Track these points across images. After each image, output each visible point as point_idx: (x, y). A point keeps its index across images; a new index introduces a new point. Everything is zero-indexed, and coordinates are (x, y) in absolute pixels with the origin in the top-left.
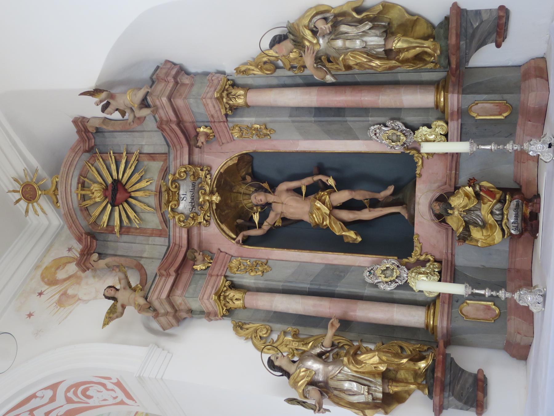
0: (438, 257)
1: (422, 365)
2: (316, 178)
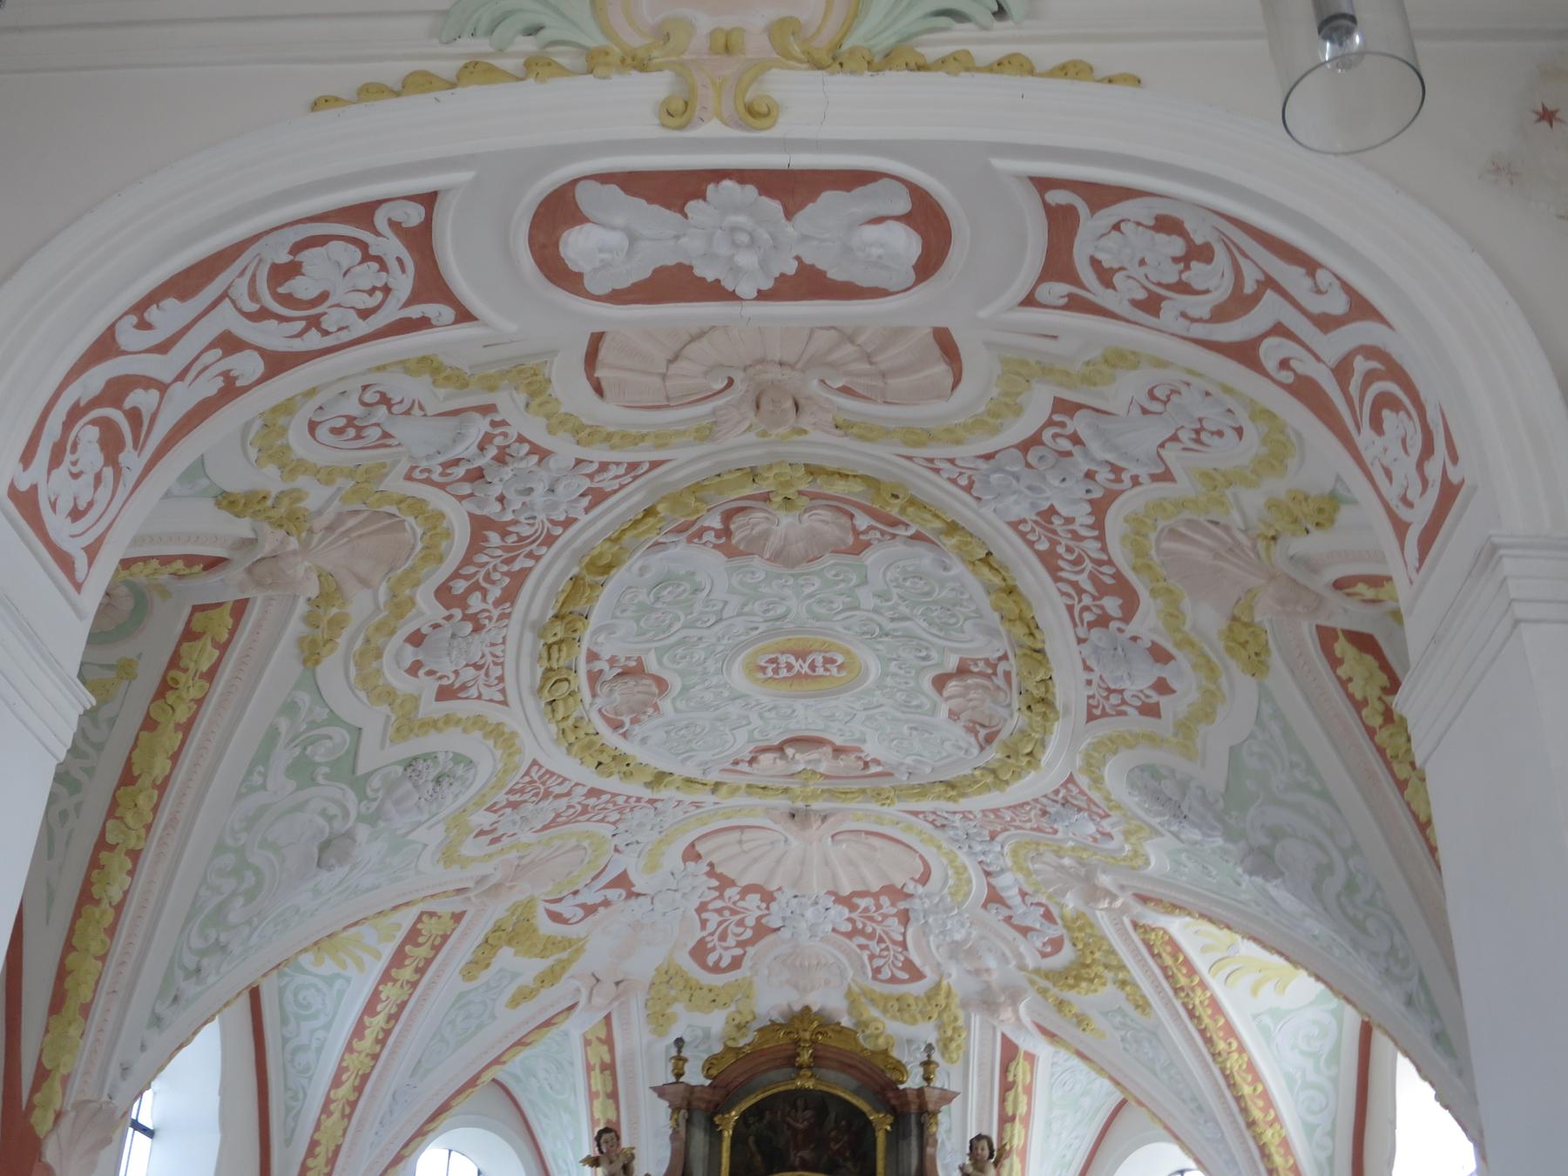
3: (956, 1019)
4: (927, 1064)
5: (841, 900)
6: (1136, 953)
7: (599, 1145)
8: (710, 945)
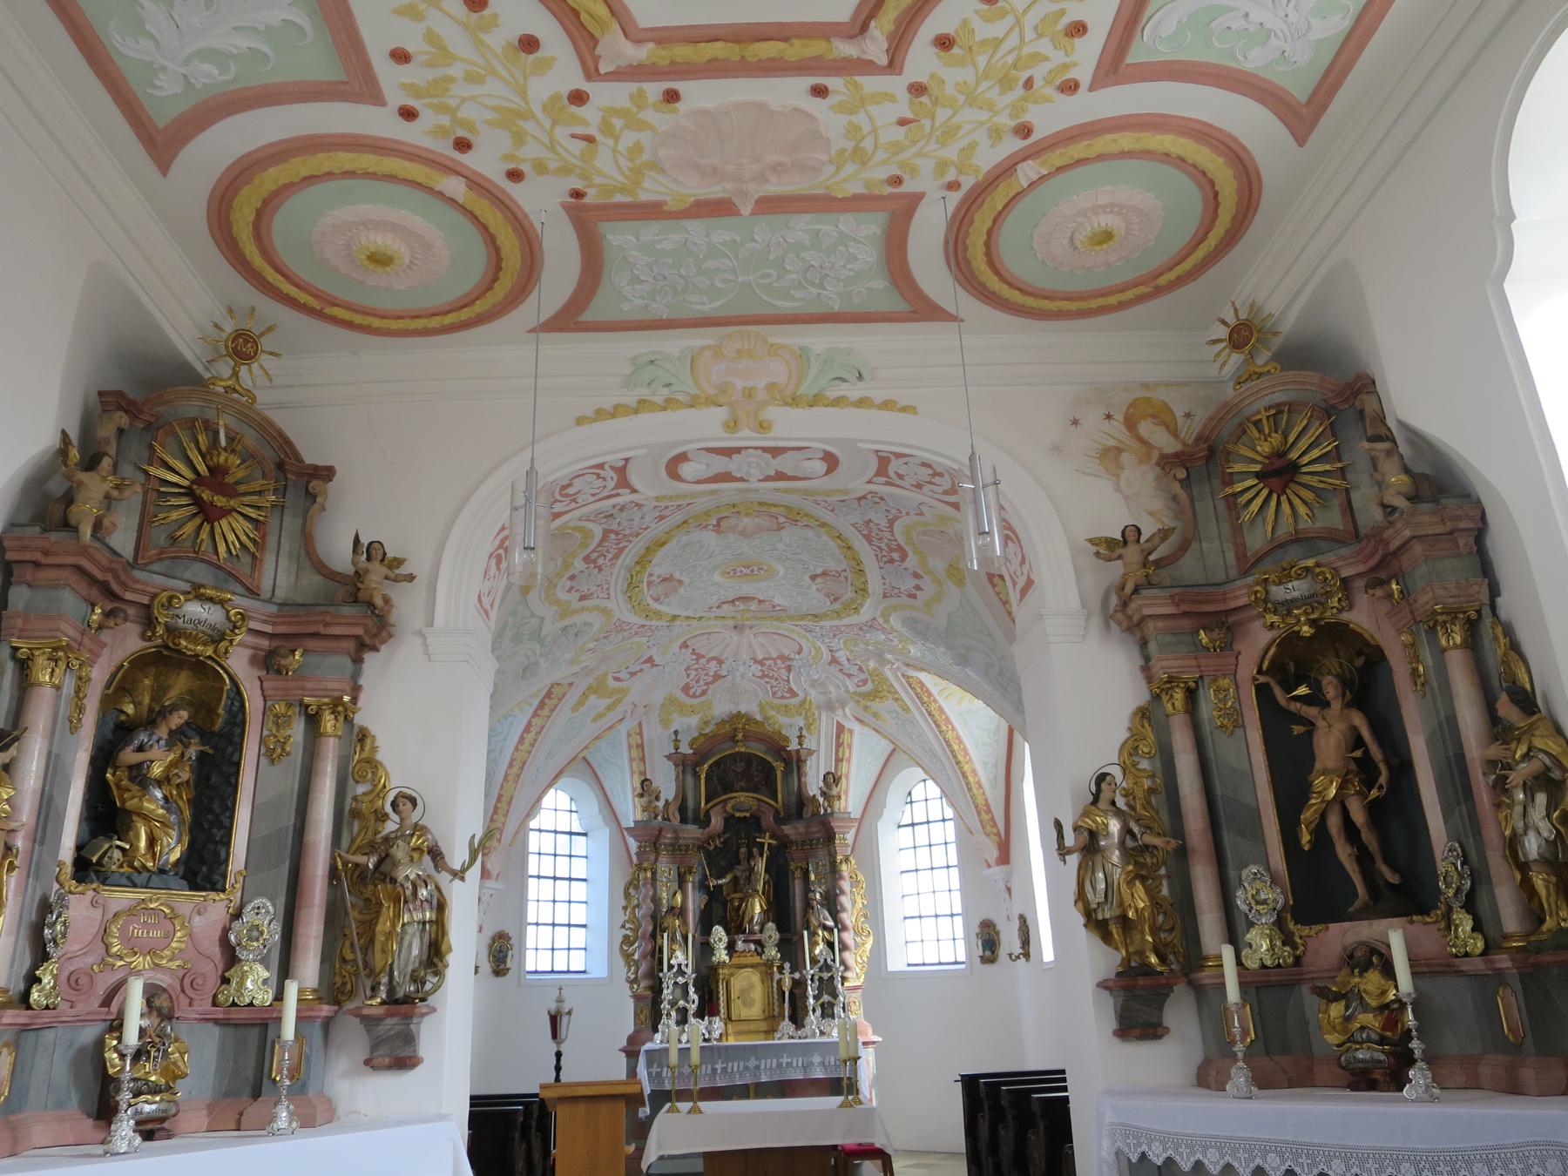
0: (1306, 960)
1: (1153, 959)
2: (1382, 766)
4: (800, 737)
5: (756, 661)
6: (903, 687)
7: (643, 788)
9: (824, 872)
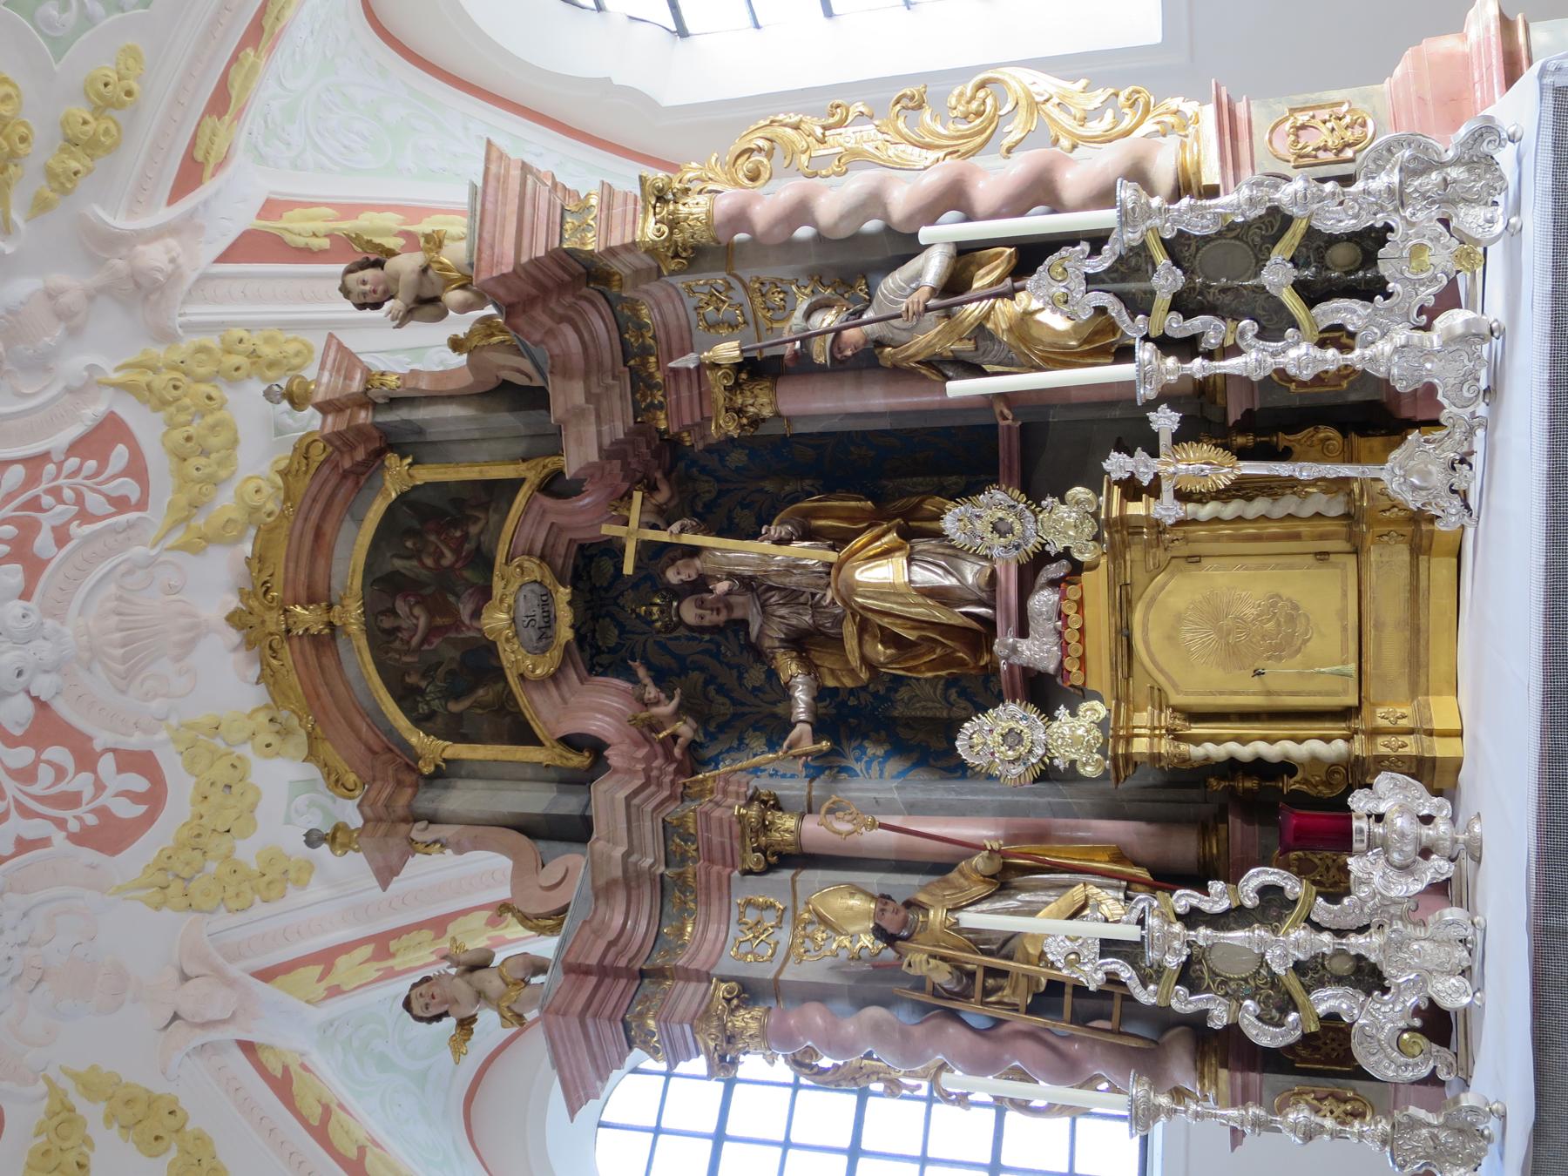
3: (203, 349)
8: (91, 820)
9: (739, 295)
